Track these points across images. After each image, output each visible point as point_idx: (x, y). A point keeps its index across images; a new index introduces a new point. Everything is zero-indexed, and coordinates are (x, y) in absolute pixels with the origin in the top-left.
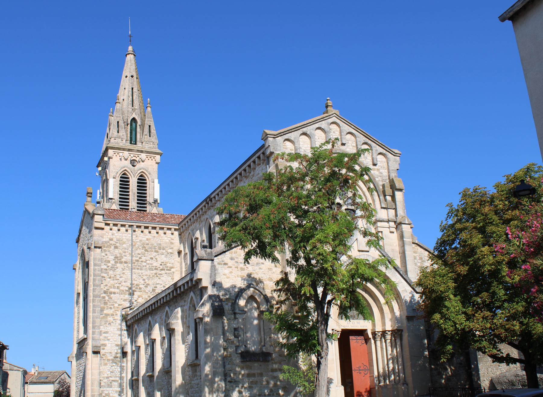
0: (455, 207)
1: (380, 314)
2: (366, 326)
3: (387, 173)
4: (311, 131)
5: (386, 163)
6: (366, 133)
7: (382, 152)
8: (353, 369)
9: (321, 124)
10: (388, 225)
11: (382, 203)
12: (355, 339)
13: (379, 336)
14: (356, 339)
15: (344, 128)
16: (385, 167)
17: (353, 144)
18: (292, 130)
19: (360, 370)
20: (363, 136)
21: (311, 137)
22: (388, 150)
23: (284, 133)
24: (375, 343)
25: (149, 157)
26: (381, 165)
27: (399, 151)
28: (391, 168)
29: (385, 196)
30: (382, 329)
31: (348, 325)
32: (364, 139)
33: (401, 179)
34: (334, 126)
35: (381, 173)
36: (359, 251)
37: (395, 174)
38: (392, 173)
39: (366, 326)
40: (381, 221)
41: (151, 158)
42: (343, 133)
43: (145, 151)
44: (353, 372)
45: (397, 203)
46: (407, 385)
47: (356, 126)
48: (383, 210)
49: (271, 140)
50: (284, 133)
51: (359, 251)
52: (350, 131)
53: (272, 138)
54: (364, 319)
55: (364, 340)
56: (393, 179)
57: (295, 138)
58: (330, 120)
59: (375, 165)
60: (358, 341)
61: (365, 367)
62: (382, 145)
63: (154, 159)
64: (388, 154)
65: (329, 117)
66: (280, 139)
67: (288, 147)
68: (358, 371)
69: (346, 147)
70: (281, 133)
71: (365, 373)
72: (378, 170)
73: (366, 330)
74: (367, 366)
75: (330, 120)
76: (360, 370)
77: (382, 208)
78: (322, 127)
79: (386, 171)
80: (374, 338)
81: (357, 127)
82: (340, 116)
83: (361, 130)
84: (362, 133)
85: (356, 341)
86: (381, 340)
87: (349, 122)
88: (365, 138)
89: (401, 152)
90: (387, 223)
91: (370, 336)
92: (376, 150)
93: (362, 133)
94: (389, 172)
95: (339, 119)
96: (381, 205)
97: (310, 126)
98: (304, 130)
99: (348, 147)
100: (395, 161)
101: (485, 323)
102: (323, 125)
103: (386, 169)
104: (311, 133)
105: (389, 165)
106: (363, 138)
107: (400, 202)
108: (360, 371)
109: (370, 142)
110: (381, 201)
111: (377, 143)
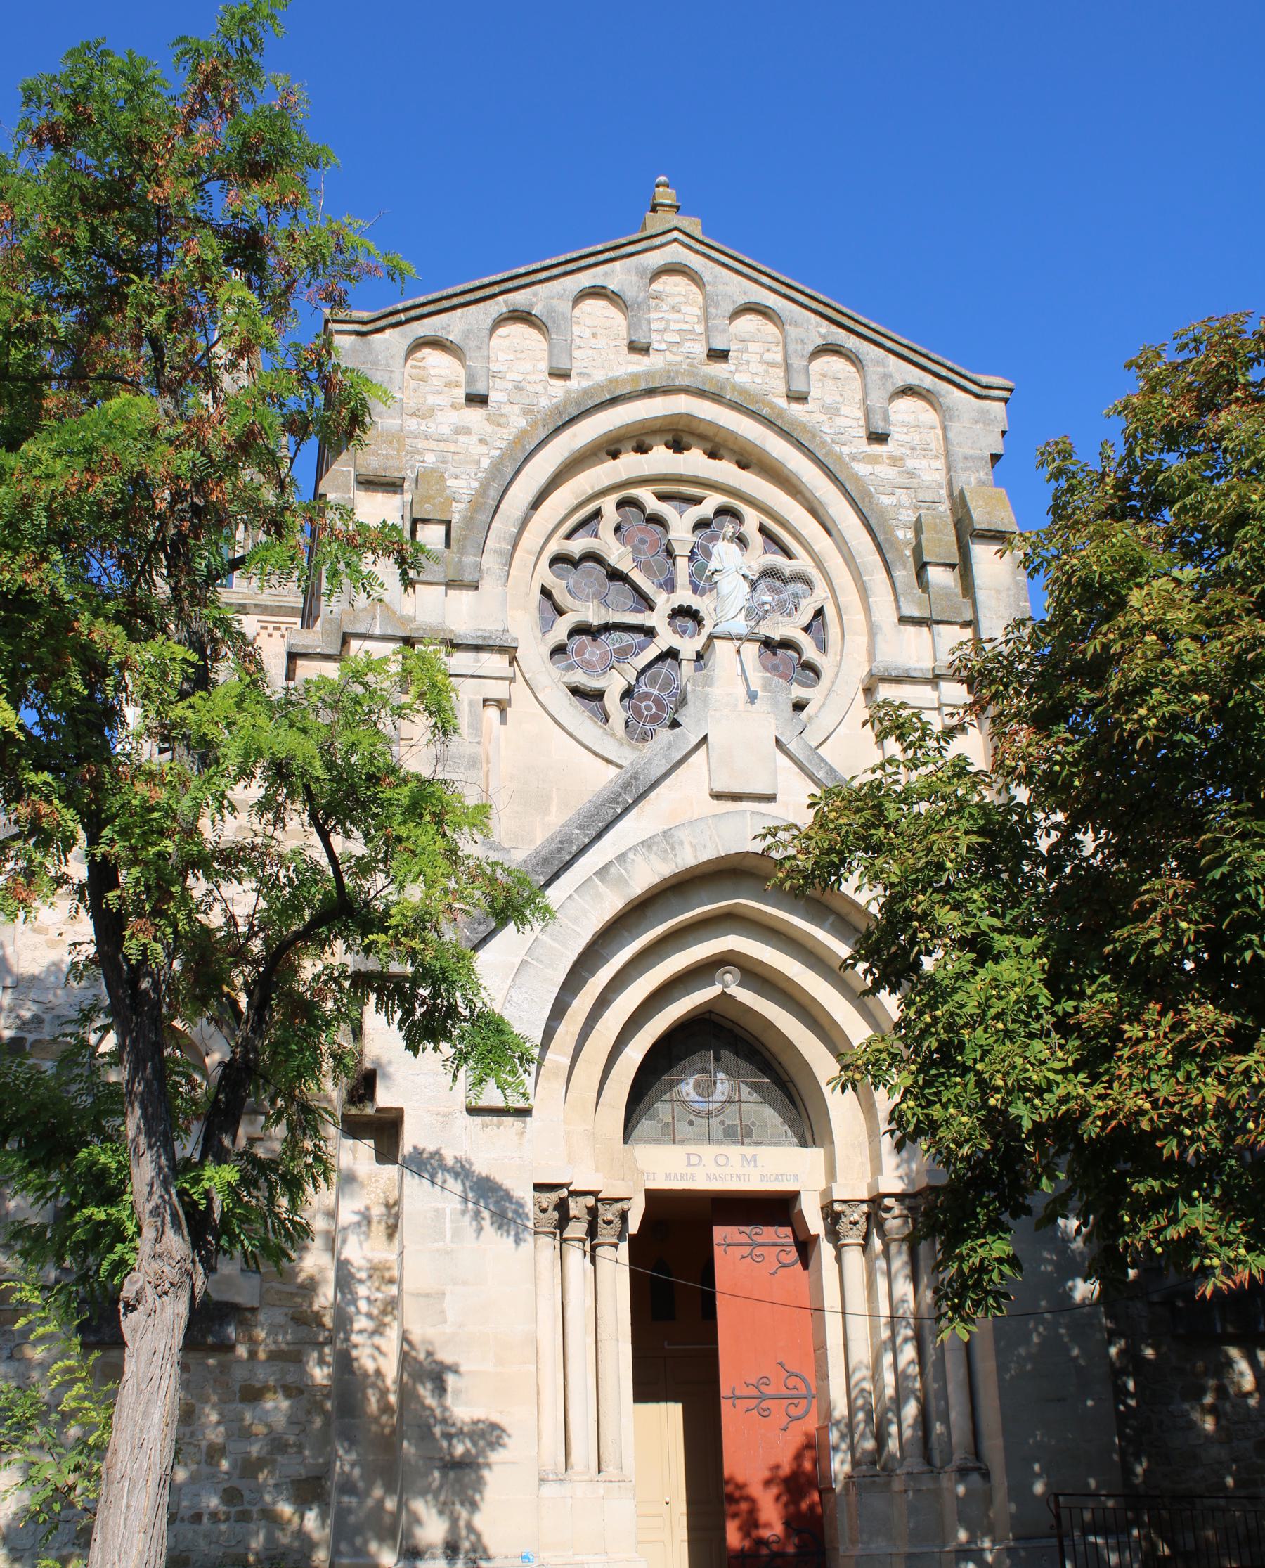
0: (1087, 458)
1: (861, 1115)
2: (796, 1177)
3: (944, 472)
4: (555, 302)
5: (940, 432)
6: (833, 303)
7: (916, 382)
8: (724, 1390)
9: (606, 274)
10: (935, 694)
11: (902, 599)
12: (745, 1239)
13: (855, 1223)
14: (746, 1240)
15: (721, 288)
16: (933, 446)
17: (768, 357)
18: (455, 301)
19: (763, 1397)
20: (819, 319)
21: (549, 325)
22: (944, 372)
23: (413, 313)
24: (839, 1259)
25: (271, 626)
26: (915, 438)
27: (1004, 377)
28: (958, 451)
29: (921, 567)
30: (870, 1191)
31: (690, 1170)
32: (823, 331)
33: (1003, 490)
34: (673, 285)
35: (911, 475)
36: (717, 796)
37: (982, 475)
38: (967, 469)
39: (796, 1177)
40: (898, 680)
41: (279, 629)
42: (717, 307)
43: (256, 605)
44: (725, 1406)
45: (981, 596)
46: (986, 1475)
47: (783, 278)
48: (910, 630)
49: (347, 346)
50: (413, 313)
51: (717, 796)
52: (752, 300)
53: (353, 337)
54: (803, 1143)
55: (794, 1249)
56: (962, 492)
57: (467, 335)
58: (655, 259)
59: (879, 438)
60: (758, 1251)
61: (792, 1382)
62: (915, 351)
63: (277, 634)
64: (948, 392)
65: (649, 242)
66: (392, 341)
67: (433, 372)
68: (755, 1402)
69: (733, 368)
70: (397, 312)
71: (794, 1412)
72: (895, 461)
73: (794, 1196)
74: (804, 1380)
75: (655, 259)
76: (763, 1397)
77: (903, 620)
78: (611, 287)
79: (940, 464)
80: (834, 1236)
81: (789, 281)
82: (707, 240)
83: (809, 291)
84: (814, 305)
85: (746, 1250)
86: (865, 1246)
87: (747, 260)
88: (825, 328)
89: (1011, 380)
90: (928, 688)
91: (815, 1224)
92: (886, 377)
93: (814, 305)
94: (949, 469)
95: (697, 252)
96: (898, 608)
97: (550, 284)
98: (519, 299)
99: (745, 367)
100: (984, 419)
101: (1188, 1077)
102: (616, 275)
103: (937, 457)
104: (551, 310)
105: (951, 435)
106: (818, 325)
107: (998, 592)
108: (765, 1405)
109: (851, 342)
110: (899, 590)
111: (889, 344)
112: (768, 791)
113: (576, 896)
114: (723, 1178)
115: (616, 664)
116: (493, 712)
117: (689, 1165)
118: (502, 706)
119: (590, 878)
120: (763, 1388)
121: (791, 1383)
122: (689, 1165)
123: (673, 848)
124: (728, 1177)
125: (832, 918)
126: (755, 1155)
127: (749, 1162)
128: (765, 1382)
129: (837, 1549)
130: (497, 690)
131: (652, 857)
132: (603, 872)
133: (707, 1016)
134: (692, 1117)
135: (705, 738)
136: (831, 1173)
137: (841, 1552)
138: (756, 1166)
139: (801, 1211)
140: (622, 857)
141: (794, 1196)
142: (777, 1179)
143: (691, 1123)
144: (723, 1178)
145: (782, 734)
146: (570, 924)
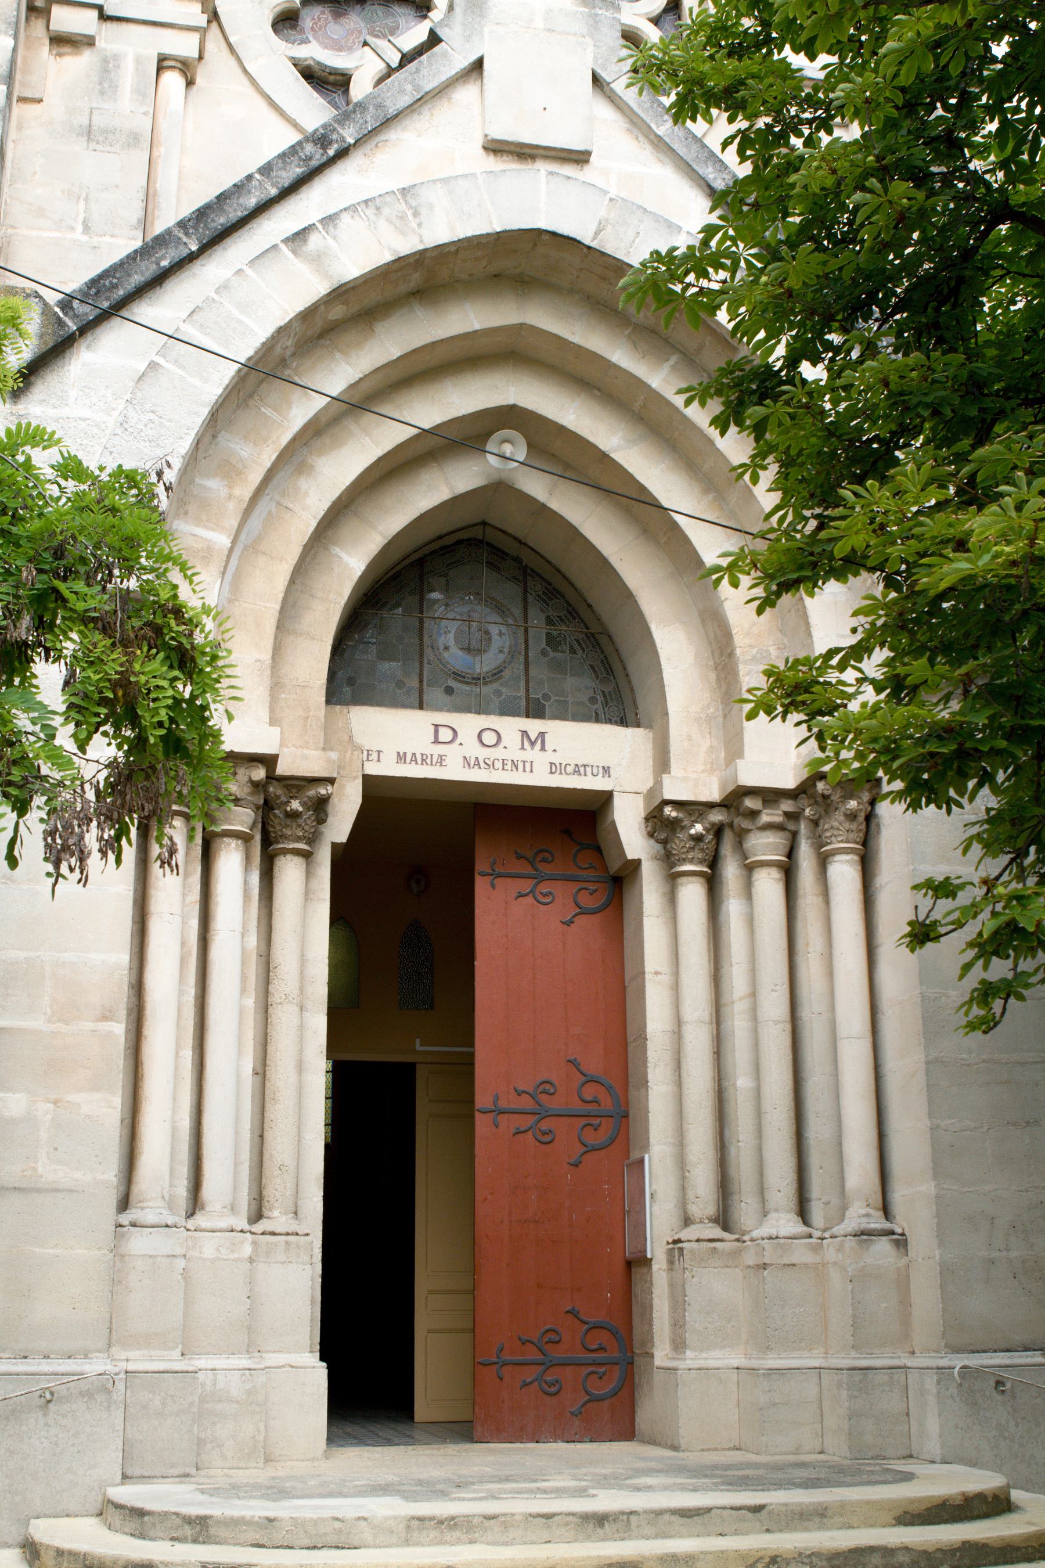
2: (606, 770)
39: (606, 770)
68: (531, 1120)
71: (592, 1138)
73: (606, 798)
76: (541, 1113)
108: (544, 1126)
112: (576, 144)
113: (249, 271)
114: (490, 765)
115: (370, 39)
116: (173, 80)
117: (436, 741)
118: (188, 69)
119: (275, 247)
120: (544, 1099)
121: (590, 1092)
122: (436, 741)
123: (416, 214)
124: (498, 765)
125: (673, 359)
126: (542, 735)
127: (533, 744)
128: (546, 1087)
129: (652, 1356)
130: (185, 46)
131: (382, 223)
132: (299, 237)
133: (477, 533)
134: (452, 683)
135: (478, 65)
136: (662, 763)
137: (658, 1361)
138: (543, 748)
139: (613, 823)
140: (329, 220)
141: (606, 798)
142: (577, 771)
143: (449, 691)
144: (490, 765)
145: (604, 68)
146: (236, 313)
